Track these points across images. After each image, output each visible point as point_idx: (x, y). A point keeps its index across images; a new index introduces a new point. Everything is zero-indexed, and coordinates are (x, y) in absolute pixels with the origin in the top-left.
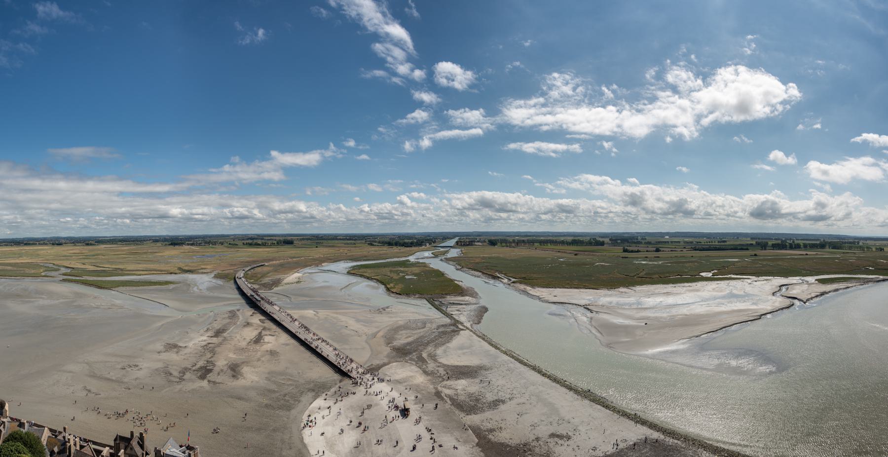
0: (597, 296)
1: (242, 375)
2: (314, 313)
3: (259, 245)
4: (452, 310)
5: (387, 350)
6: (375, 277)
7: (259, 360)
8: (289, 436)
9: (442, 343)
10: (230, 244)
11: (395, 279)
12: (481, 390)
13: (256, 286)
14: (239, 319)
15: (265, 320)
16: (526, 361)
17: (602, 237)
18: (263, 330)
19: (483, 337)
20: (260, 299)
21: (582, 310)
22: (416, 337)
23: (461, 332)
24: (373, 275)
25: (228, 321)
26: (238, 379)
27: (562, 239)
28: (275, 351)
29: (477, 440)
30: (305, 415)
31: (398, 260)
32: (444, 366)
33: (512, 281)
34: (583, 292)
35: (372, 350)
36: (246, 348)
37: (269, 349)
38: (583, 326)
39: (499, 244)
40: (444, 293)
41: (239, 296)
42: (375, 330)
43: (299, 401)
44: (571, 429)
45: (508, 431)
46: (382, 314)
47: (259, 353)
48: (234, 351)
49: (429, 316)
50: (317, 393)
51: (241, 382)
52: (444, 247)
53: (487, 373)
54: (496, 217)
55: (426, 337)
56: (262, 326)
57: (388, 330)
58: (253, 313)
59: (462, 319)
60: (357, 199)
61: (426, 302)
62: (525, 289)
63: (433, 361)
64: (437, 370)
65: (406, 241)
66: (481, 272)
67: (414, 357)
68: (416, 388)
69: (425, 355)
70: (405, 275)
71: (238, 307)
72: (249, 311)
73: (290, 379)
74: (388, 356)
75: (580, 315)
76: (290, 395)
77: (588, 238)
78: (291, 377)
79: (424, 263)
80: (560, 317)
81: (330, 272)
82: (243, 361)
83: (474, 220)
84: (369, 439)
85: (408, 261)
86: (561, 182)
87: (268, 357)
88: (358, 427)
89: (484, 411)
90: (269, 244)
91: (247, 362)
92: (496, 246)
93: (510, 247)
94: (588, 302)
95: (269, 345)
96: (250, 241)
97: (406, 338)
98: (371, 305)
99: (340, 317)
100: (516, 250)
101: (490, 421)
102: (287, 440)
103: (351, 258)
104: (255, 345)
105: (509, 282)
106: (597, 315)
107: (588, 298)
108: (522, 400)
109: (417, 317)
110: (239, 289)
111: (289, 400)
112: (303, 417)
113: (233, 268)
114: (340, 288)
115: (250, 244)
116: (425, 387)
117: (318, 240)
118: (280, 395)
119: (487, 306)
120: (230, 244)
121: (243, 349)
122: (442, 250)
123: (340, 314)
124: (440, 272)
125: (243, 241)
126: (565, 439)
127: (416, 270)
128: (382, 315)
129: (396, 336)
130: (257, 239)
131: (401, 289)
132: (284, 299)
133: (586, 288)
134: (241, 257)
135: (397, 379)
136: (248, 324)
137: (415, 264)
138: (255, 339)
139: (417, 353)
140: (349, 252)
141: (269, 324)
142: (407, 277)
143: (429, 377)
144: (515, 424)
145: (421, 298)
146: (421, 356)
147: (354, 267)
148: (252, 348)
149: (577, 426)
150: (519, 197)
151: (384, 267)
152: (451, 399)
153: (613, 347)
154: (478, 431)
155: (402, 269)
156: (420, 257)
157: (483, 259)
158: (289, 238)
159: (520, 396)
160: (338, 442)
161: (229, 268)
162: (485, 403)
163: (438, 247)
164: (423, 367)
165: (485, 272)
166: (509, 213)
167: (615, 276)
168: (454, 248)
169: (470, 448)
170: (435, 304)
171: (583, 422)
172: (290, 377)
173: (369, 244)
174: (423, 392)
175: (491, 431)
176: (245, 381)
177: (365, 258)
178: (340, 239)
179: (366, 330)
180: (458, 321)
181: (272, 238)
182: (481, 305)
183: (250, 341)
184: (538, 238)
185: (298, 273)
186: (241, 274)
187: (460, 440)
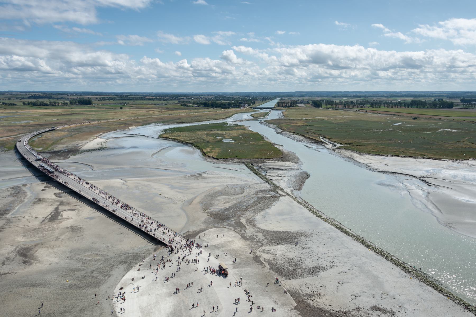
0: (438, 167)
1: (35, 259)
3: (46, 105)
4: (271, 175)
5: (204, 216)
6: (190, 141)
7: (57, 239)
8: (99, 312)
9: (262, 208)
12: (300, 256)
14: (26, 195)
15: (61, 193)
16: (350, 231)
17: (450, 98)
18: (60, 205)
19: (304, 204)
20: (53, 170)
21: (418, 182)
22: (234, 202)
23: (281, 198)
24: (188, 138)
25: (11, 199)
27: (399, 99)
28: (77, 227)
29: (296, 304)
30: (117, 288)
31: (215, 123)
32: (263, 231)
33: (336, 147)
34: (420, 162)
35: (188, 217)
36: (39, 228)
37: (69, 226)
38: (417, 200)
39: (324, 106)
40: (263, 158)
41: (24, 169)
42: (191, 197)
43: (110, 276)
44: (395, 306)
45: (328, 297)
46: (198, 179)
48: (23, 233)
49: (248, 181)
50: (129, 264)
51: (35, 267)
52: (264, 108)
53: (307, 239)
54: (326, 75)
55: (245, 202)
56: (58, 201)
58: (45, 187)
59: (282, 184)
60: (179, 53)
61: (245, 167)
62: (351, 155)
63: (252, 226)
64: (256, 235)
65: (223, 102)
66: (304, 136)
67: (233, 223)
68: (235, 254)
69: (243, 220)
71: (23, 182)
72: (39, 185)
74: (205, 222)
75: (414, 188)
76: (98, 271)
77: (432, 99)
78: (99, 251)
79: (243, 126)
80: (391, 188)
81: (138, 136)
82: (37, 243)
83: (300, 79)
84: (186, 304)
85: (226, 123)
86: (421, 30)
87: (68, 234)
88: (176, 293)
89: (303, 276)
90: (60, 104)
91: (42, 244)
92: (320, 108)
93: (336, 109)
94: (425, 174)
95: (68, 221)
96: (34, 100)
97: (224, 203)
98: (186, 171)
99: (152, 184)
100: (343, 112)
101: (309, 287)
103: (162, 121)
104: (51, 223)
105: (334, 148)
106: (436, 189)
107: (426, 169)
108: (344, 269)
109: (235, 182)
110: (22, 159)
111: (97, 276)
112: (115, 291)
115: (34, 104)
116: (243, 252)
117: (122, 99)
118: (87, 273)
119: (309, 172)
121: (35, 229)
122: (262, 111)
123: (152, 181)
124: (260, 135)
125: (23, 100)
126: (388, 314)
127: (234, 133)
128: (198, 181)
129: (214, 202)
131: (218, 153)
132: (85, 168)
133: (424, 158)
135: (214, 244)
136: (39, 200)
137: (233, 127)
138: (50, 216)
139: (235, 218)
140: (160, 113)
141: (67, 198)
142: (224, 141)
143: (248, 243)
144: (335, 292)
145: (239, 162)
146: (240, 221)
147: (166, 131)
149: (403, 304)
150: (360, 51)
151: (200, 130)
152: (270, 263)
153: (452, 227)
154: (297, 295)
155: (219, 132)
156: (238, 120)
157: (306, 122)
158: (86, 97)
159: (341, 265)
161: (5, 135)
162: (304, 269)
163: (258, 108)
164: (242, 233)
165: (307, 136)
166: (341, 71)
167: (464, 146)
168: (274, 110)
169: (288, 310)
170: (254, 169)
171: (410, 300)
172: (97, 253)
173: (182, 105)
174: (242, 257)
175: (310, 296)
176: (40, 265)
177: (178, 121)
179: (181, 196)
180: (278, 187)
181: (62, 96)
182: (301, 171)
184: (369, 99)
186: (25, 139)
187: (279, 303)
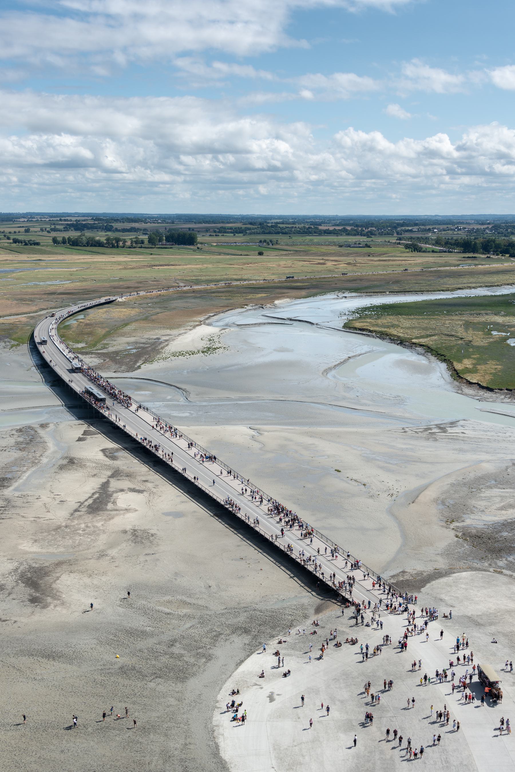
1: (55, 597)
2: (252, 432)
3: (99, 244)
6: (422, 341)
7: (102, 555)
8: (182, 741)
10: (15, 241)
11: (478, 347)
13: (90, 361)
14: (45, 449)
15: (117, 450)
18: (112, 476)
20: (102, 396)
24: (416, 333)
25: (16, 454)
26: (45, 606)
28: (144, 531)
31: (489, 293)
35: (404, 535)
36: (66, 527)
37: (128, 527)
41: (45, 388)
42: (414, 483)
43: (209, 658)
46: (436, 440)
47: (103, 539)
50: (255, 637)
57: (453, 485)
58: (85, 433)
70: (507, 338)
71: (42, 419)
73: (185, 603)
74: (447, 553)
76: (184, 642)
78: (190, 596)
81: (295, 323)
82: (61, 559)
84: (388, 757)
87: (126, 547)
90: (128, 243)
96: (74, 234)
98: (407, 415)
102: (176, 753)
104: (91, 516)
111: (182, 655)
112: (219, 697)
113: (25, 309)
114: (322, 369)
115: (74, 243)
117: (264, 233)
118: (159, 644)
120: (15, 241)
121: (59, 527)
123: (321, 436)
125: (54, 234)
129: (473, 502)
130: (91, 227)
131: (494, 374)
132: (169, 394)
134: (49, 279)
138: (90, 501)
147: (362, 313)
148: (83, 526)
155: (499, 319)
160: (307, 758)
161: (14, 311)
172: (184, 598)
173: (407, 247)
176: (64, 611)
178: (328, 232)
183: (76, 506)
185: (209, 325)
